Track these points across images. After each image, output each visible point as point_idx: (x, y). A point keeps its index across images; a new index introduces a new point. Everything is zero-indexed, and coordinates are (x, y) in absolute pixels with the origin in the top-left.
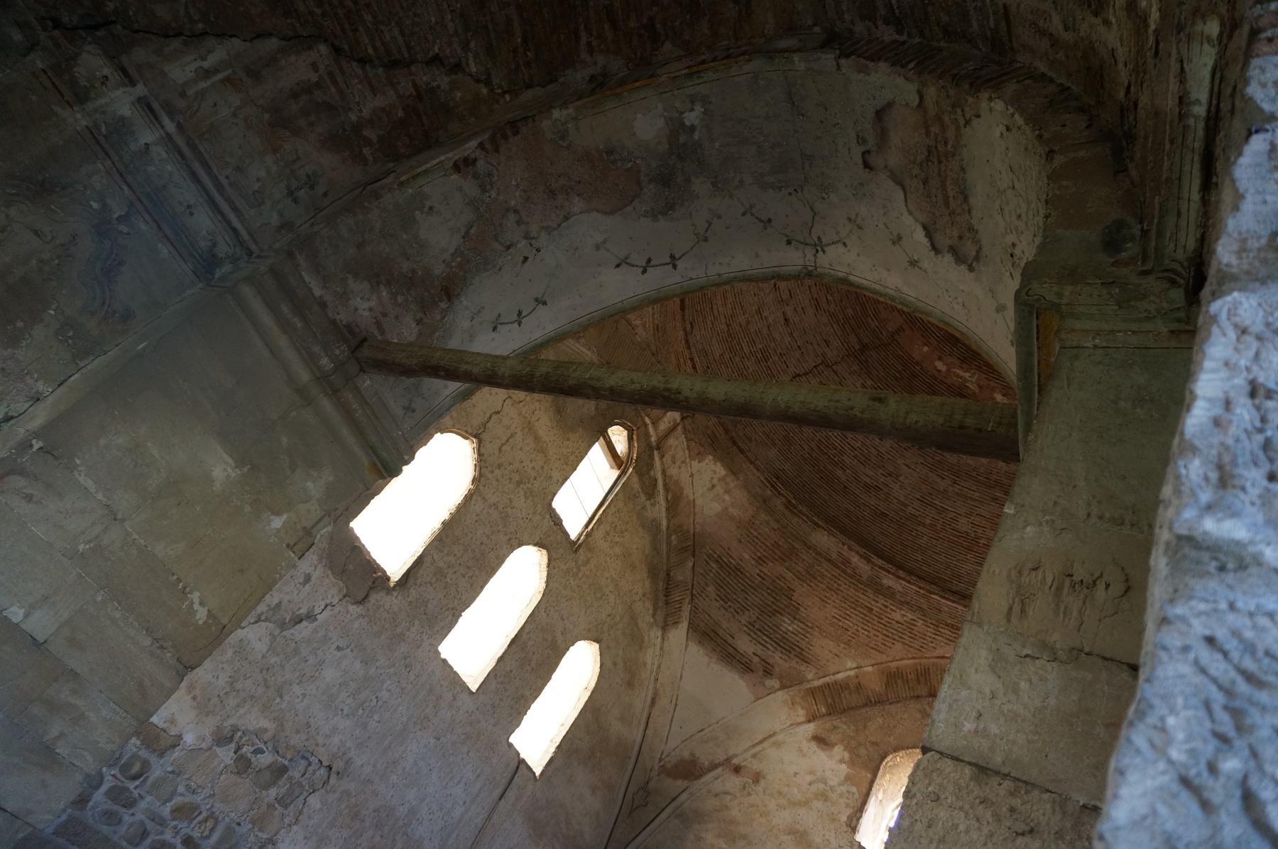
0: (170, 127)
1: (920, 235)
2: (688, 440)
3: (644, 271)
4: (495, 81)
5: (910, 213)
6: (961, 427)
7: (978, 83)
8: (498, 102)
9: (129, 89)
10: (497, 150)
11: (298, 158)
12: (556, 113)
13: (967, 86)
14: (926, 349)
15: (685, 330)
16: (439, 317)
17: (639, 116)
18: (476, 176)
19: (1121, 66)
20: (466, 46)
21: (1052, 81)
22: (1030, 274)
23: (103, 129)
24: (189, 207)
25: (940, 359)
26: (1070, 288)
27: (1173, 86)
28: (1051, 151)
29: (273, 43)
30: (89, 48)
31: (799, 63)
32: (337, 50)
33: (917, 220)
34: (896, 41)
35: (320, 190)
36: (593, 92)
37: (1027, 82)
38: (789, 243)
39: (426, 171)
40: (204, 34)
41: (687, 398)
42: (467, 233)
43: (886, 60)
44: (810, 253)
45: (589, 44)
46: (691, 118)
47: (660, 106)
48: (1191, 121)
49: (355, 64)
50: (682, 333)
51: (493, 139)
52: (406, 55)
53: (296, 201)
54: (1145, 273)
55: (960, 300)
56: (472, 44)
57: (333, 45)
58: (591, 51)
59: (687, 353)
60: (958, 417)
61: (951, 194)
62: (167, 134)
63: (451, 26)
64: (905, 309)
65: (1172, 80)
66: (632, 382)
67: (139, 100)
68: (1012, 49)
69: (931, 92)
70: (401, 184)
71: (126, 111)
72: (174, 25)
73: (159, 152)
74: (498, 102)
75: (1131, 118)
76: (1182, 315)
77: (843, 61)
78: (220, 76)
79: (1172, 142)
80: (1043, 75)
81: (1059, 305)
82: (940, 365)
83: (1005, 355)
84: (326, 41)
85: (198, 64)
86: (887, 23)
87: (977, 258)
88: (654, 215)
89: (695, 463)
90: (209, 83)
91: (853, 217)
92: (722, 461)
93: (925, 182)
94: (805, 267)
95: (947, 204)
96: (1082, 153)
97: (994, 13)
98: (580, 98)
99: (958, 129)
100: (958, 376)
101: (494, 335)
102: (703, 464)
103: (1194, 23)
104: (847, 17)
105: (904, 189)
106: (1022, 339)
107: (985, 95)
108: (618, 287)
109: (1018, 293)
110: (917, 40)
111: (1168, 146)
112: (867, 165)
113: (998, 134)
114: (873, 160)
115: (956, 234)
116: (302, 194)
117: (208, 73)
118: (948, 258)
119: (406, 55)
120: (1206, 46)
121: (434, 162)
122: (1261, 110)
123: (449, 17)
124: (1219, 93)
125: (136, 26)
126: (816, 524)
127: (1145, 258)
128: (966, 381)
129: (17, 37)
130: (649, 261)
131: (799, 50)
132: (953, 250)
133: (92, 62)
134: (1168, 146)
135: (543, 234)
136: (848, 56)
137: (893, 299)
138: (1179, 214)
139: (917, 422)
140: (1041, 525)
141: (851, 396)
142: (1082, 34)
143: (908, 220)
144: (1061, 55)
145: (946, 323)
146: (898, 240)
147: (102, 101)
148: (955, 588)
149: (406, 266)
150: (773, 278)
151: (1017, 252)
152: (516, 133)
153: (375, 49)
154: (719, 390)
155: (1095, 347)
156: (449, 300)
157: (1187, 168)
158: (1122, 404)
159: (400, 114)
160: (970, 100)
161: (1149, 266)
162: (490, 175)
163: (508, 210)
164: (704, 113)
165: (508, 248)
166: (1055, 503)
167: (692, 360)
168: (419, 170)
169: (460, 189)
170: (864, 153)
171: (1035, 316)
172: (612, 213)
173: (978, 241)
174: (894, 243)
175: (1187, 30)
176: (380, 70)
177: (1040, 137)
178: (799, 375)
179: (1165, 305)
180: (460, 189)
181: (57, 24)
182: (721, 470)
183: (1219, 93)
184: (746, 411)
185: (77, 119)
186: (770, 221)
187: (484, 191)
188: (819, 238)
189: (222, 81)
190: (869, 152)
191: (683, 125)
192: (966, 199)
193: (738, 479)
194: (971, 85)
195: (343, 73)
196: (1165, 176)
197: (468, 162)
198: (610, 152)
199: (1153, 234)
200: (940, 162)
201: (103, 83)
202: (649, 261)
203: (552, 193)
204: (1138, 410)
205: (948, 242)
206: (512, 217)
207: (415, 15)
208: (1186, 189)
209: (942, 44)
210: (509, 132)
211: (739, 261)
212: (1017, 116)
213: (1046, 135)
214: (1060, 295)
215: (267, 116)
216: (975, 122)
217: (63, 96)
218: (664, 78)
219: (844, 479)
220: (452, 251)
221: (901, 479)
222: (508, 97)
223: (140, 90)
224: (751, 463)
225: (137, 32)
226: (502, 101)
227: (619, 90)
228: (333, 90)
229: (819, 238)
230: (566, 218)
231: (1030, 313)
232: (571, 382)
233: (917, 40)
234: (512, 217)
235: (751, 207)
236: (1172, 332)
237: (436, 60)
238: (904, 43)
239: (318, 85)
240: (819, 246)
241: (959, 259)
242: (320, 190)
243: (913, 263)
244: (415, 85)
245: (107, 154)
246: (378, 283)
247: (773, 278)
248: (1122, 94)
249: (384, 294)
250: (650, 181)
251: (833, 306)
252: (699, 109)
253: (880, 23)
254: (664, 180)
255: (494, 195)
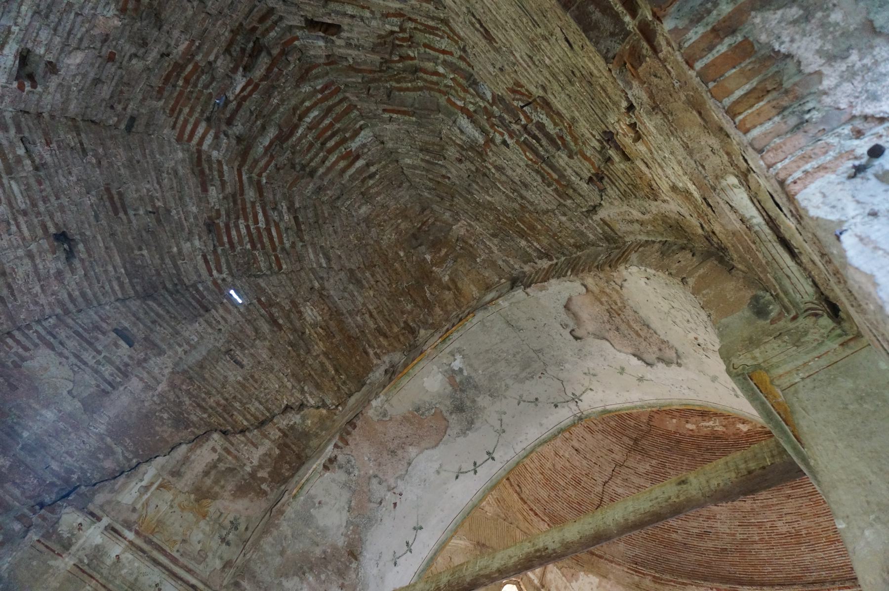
0: (131, 536)
1: (634, 360)
2: (560, 569)
3: (476, 472)
4: (328, 402)
5: (620, 351)
6: (750, 472)
7: (613, 263)
8: (335, 414)
9: (98, 524)
10: (347, 444)
11: (222, 513)
12: (374, 403)
13: (608, 268)
14: (674, 421)
15: (516, 492)
16: (354, 576)
17: (425, 379)
18: (340, 467)
19: (688, 218)
20: (302, 391)
21: (654, 242)
22: (726, 355)
23: (86, 561)
24: (157, 585)
25: (687, 422)
26: (758, 350)
27: (733, 217)
28: (683, 279)
29: (184, 448)
30: (67, 510)
31: (503, 303)
32: (225, 433)
33: (627, 353)
34: (551, 265)
35: (242, 527)
36: (390, 379)
37: (640, 249)
38: (556, 406)
39: (307, 480)
40: (139, 464)
41: (554, 550)
42: (350, 507)
43: (553, 277)
44: (573, 405)
45: (376, 354)
46: (457, 364)
47: (435, 367)
48: (757, 228)
49: (238, 436)
50: (515, 495)
51: (342, 438)
52: (268, 414)
53: (228, 544)
54: (795, 318)
55: (684, 386)
56: (306, 388)
57: (221, 431)
58: (378, 356)
59: (525, 507)
60: (743, 466)
61: (637, 328)
62: (129, 541)
63: (289, 385)
64: (654, 409)
65: (728, 213)
66: (511, 557)
67: (106, 528)
68: (620, 237)
69: (590, 281)
70: (295, 497)
71: (98, 540)
72: (117, 469)
73: (129, 556)
74: (335, 414)
75: (715, 239)
76: (839, 331)
77: (528, 290)
78: (155, 486)
79: (754, 243)
80: (647, 241)
81: (759, 364)
82: (690, 426)
83: (737, 403)
84: (216, 430)
85: (140, 484)
86: (540, 258)
87: (678, 357)
88: (463, 433)
89: (574, 584)
90: (149, 494)
91: (586, 371)
92: (592, 572)
93: (617, 329)
94: (575, 415)
95: (639, 335)
96: (701, 271)
97: (598, 225)
98: (384, 387)
99: (617, 292)
100: (706, 427)
101: (396, 569)
102: (580, 581)
103: (720, 183)
104: (516, 266)
105: (607, 340)
106: (753, 398)
107: (621, 268)
108: (464, 491)
109: (728, 372)
110: (563, 259)
111: (753, 246)
112: (576, 338)
113: (644, 284)
114: (578, 333)
115: (655, 349)
116: (231, 537)
117: (147, 488)
118: (661, 365)
119: (268, 414)
120: (735, 190)
121: (310, 472)
122: (832, 222)
123: (286, 380)
124: (763, 208)
125: (94, 481)
126: (683, 584)
127: (788, 312)
128: (713, 427)
129: (17, 527)
130: (475, 464)
131: (499, 297)
132: (660, 359)
133: (70, 518)
134: (753, 246)
135: (399, 482)
136: (529, 286)
137: (642, 407)
138: (788, 277)
139: (718, 484)
140: (872, 525)
141: (667, 491)
142: (655, 212)
143: (621, 356)
144: (650, 227)
145: (685, 405)
146: (622, 370)
147: (81, 542)
148: (811, 579)
149: (318, 551)
150: (559, 433)
151: (701, 341)
152: (355, 427)
153: (247, 420)
154: (573, 532)
155: (803, 379)
156: (356, 559)
157: (773, 251)
158: (851, 407)
159: (277, 452)
160: (615, 274)
161: (793, 314)
162: (349, 461)
163: (370, 478)
164: (463, 357)
165: (381, 503)
166: (868, 503)
167: (531, 510)
168: (303, 481)
169: (333, 480)
170: (571, 333)
171: (748, 379)
172: (437, 445)
173: (673, 347)
174: (621, 373)
175: (719, 188)
176: (255, 432)
177: (670, 274)
178: (606, 482)
179: (822, 331)
180: (333, 480)
181: (42, 505)
182: (594, 579)
183: (763, 208)
184: (599, 538)
185: (66, 563)
186: (537, 399)
187: (349, 473)
188: (573, 394)
189: (158, 488)
190: (573, 330)
191: (453, 371)
192: (648, 326)
193: (610, 579)
194: (610, 266)
195: (233, 445)
196: (764, 262)
197: (332, 460)
198: (418, 410)
199: (782, 295)
200: (619, 315)
201: (79, 529)
202: (475, 464)
203: (393, 452)
204: (865, 406)
205: (654, 356)
206: (374, 481)
207: (265, 389)
208: (781, 262)
209: (579, 253)
210: (350, 429)
211: (531, 433)
212: (648, 270)
213: (674, 272)
214: (754, 358)
215: (193, 496)
216: (625, 284)
217: (54, 551)
218: (429, 350)
219: (680, 539)
220: (344, 524)
221: (718, 517)
222: (340, 408)
223: (105, 521)
224: (612, 562)
225: (95, 485)
226: (337, 412)
227: (405, 371)
228: (230, 458)
229: (573, 394)
230: (409, 464)
231: (745, 379)
232: (468, 580)
233: (563, 259)
234: (374, 481)
235: (521, 397)
236: (842, 345)
237: (288, 408)
238: (557, 264)
239: (220, 460)
240: (576, 399)
241: (668, 363)
242: (242, 527)
243: (641, 379)
244: (280, 430)
245: (92, 577)
246: (304, 574)
247: (559, 433)
248: (700, 231)
249: (311, 579)
250: (451, 413)
251: (600, 425)
252: (458, 357)
253: (537, 260)
254: (459, 409)
255: (356, 473)
